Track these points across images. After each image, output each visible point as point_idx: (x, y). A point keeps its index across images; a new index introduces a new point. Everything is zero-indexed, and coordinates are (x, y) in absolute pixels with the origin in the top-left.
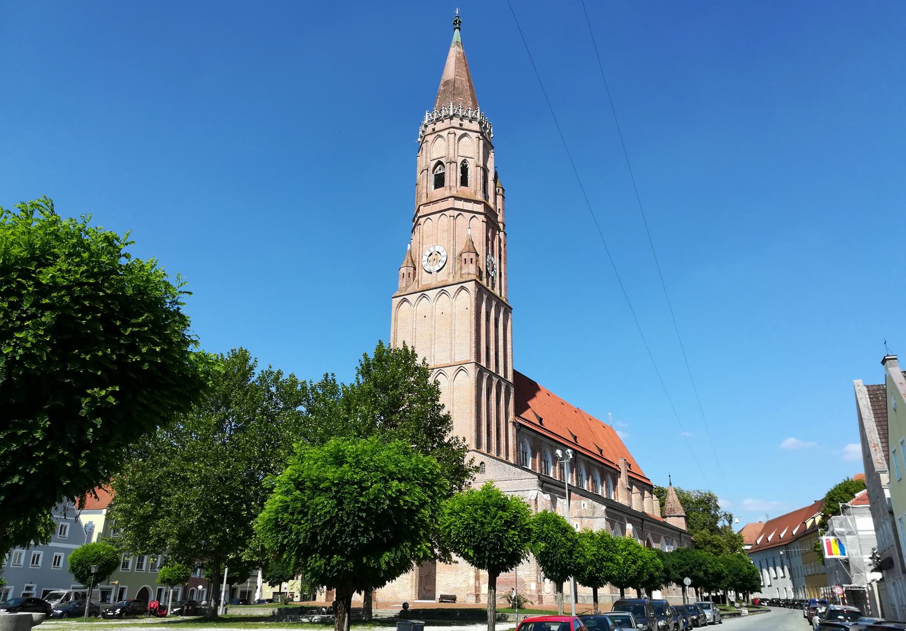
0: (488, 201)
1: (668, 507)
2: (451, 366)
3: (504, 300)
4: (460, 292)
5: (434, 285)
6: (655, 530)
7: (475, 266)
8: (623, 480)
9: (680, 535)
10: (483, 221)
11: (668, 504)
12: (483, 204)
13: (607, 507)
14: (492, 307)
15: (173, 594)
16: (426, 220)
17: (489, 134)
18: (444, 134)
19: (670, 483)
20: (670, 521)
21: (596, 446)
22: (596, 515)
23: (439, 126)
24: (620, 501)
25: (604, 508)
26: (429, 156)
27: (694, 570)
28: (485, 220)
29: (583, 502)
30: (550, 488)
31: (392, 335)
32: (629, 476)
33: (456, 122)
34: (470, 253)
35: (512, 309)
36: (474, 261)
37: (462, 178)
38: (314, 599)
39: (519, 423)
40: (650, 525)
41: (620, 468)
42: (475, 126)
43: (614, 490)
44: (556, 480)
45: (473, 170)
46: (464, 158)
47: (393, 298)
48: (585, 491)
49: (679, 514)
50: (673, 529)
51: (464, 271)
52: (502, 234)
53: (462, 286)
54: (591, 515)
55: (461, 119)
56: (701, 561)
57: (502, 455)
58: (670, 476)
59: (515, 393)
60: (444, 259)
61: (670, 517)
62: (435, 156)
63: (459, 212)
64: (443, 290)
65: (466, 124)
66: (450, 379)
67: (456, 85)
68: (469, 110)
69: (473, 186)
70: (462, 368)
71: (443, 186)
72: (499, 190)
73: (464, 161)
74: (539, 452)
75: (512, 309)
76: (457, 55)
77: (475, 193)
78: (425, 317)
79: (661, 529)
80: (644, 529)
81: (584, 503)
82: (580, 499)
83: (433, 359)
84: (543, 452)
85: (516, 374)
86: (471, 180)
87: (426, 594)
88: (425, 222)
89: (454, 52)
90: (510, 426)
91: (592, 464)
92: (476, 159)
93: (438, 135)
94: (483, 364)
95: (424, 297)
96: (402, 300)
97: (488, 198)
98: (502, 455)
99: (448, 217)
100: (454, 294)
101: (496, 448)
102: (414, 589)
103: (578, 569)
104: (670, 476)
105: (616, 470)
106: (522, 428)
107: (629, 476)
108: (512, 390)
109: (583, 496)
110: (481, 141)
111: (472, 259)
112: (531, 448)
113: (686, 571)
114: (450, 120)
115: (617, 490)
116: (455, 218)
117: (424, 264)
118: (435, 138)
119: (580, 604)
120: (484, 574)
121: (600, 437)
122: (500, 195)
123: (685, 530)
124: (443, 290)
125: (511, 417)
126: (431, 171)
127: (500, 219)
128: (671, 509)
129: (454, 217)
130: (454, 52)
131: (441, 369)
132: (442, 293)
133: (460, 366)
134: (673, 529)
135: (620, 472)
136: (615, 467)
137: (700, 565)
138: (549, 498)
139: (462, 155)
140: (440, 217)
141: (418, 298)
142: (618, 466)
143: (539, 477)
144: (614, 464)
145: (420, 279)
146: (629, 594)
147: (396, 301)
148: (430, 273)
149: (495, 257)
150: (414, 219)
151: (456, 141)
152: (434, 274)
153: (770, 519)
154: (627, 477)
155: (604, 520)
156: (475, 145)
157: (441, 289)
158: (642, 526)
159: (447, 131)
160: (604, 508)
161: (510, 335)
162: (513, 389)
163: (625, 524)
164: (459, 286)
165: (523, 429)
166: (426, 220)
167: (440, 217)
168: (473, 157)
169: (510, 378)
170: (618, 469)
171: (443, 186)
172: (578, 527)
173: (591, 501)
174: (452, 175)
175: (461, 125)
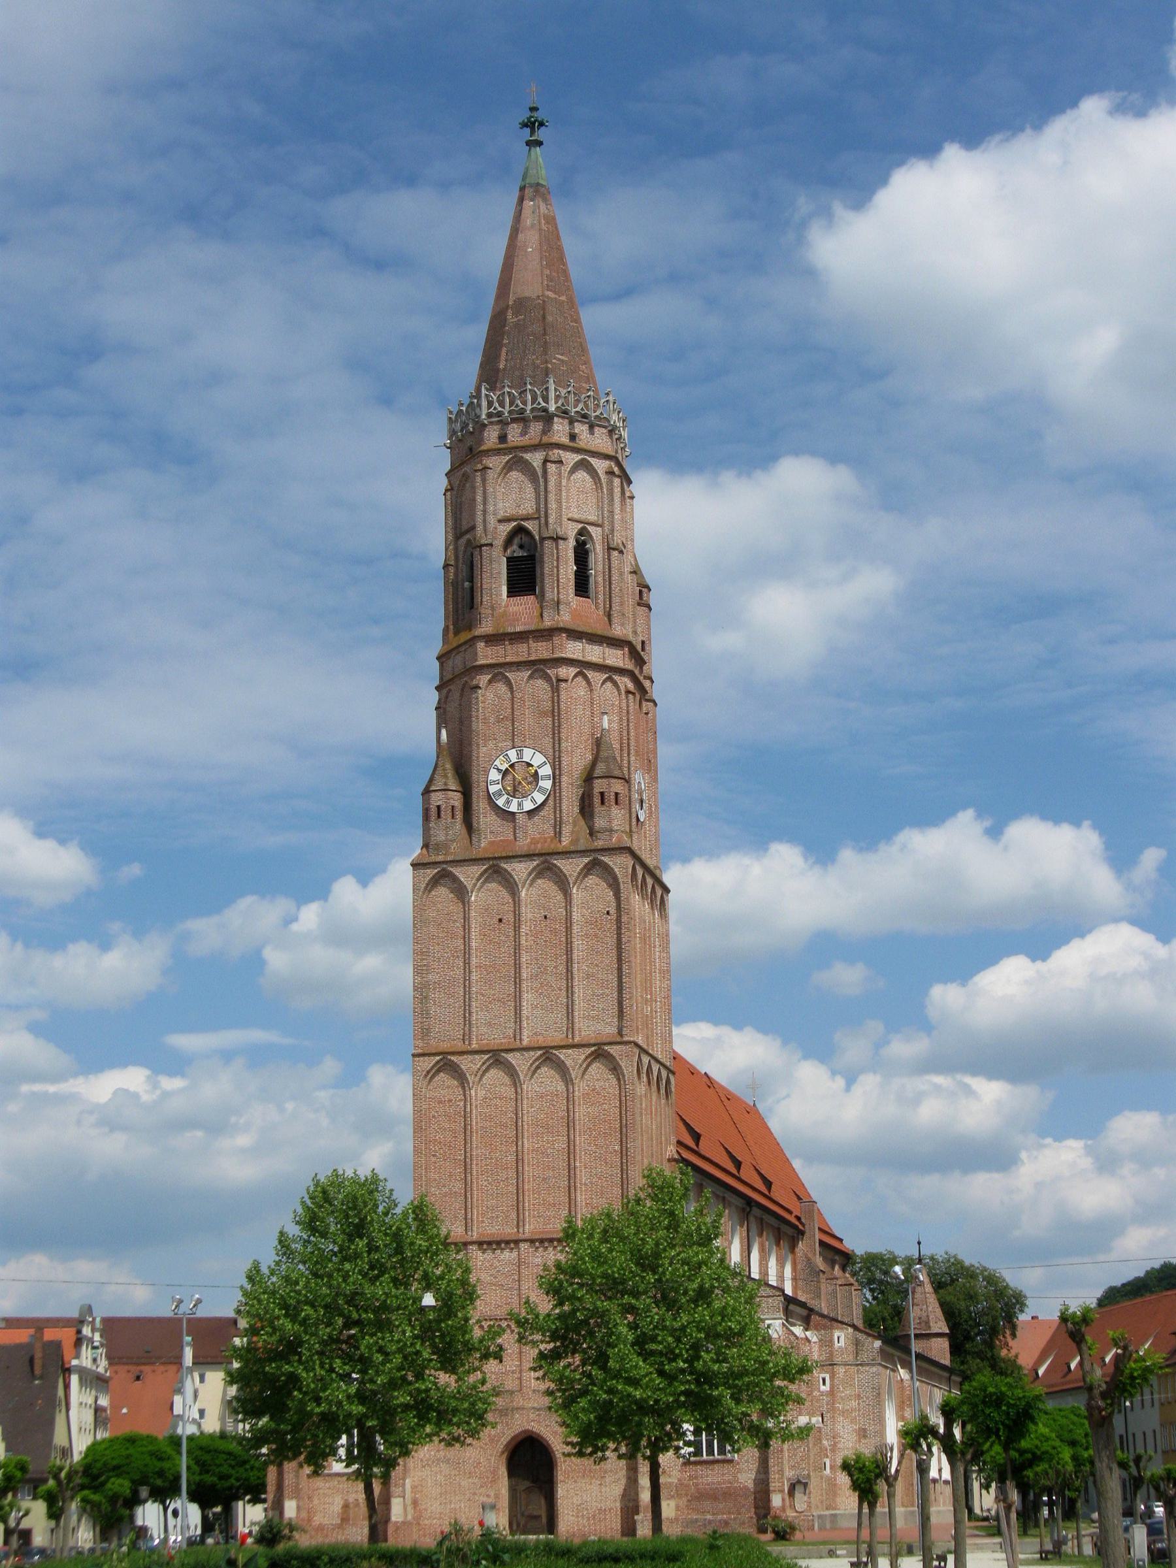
26: (491, 508)
37: (577, 574)
46: (580, 526)
51: (599, 823)
73: (582, 532)
78: (500, 920)
117: (493, 789)
175: (573, 437)
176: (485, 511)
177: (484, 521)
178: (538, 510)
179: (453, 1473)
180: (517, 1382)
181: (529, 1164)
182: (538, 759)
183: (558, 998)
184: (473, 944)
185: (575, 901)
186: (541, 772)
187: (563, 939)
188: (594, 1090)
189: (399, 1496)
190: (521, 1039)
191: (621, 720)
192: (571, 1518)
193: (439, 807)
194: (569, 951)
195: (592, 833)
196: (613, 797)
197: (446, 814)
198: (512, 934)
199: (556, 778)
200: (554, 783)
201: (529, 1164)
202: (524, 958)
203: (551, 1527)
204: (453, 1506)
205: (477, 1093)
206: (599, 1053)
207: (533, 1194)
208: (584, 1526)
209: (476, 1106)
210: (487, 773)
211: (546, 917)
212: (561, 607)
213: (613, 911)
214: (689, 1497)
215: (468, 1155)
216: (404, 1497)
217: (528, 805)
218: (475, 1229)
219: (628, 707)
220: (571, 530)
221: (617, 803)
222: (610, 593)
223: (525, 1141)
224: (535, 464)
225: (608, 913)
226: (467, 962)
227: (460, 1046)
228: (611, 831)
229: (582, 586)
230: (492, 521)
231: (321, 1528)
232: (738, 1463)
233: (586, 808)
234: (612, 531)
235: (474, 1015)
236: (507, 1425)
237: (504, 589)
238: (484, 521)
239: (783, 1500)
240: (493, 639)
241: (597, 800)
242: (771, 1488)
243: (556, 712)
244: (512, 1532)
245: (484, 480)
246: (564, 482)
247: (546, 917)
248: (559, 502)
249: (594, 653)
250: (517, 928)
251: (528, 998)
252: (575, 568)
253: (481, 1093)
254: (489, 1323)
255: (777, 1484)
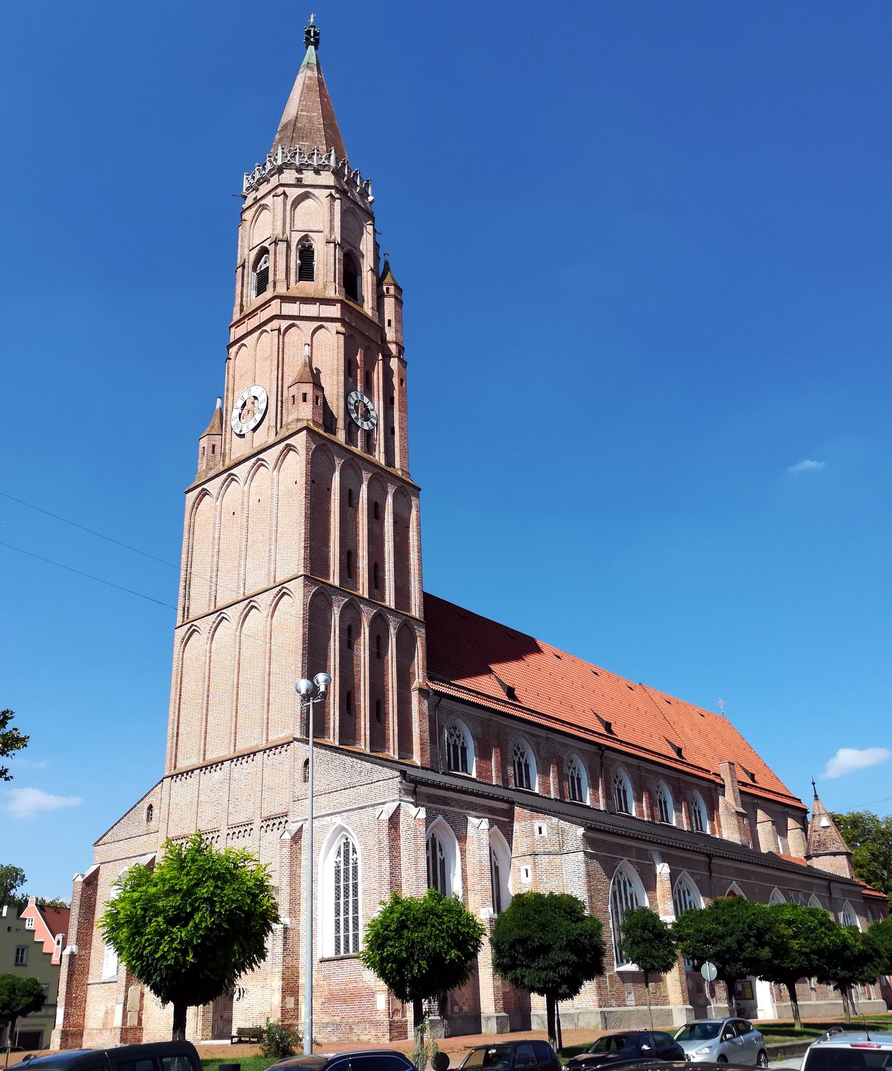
0: (362, 307)
1: (813, 839)
2: (266, 591)
3: (400, 473)
4: (285, 456)
6: (753, 878)
7: (311, 406)
8: (728, 801)
9: (829, 888)
10: (338, 333)
11: (814, 834)
12: (339, 305)
13: (588, 829)
14: (334, 471)
15: (220, 1038)
16: (239, 349)
17: (364, 194)
18: (268, 201)
19: (816, 796)
20: (822, 864)
21: (669, 742)
22: (566, 849)
23: (264, 188)
24: (725, 836)
25: (581, 831)
27: (747, 944)
28: (342, 330)
29: (537, 824)
30: (445, 798)
31: (184, 556)
32: (741, 792)
33: (289, 176)
34: (301, 385)
35: (420, 490)
36: (310, 397)
38: (479, 1032)
39: (434, 690)
40: (737, 868)
41: (722, 780)
42: (327, 178)
43: (712, 819)
44: (550, 799)
47: (187, 492)
48: (634, 818)
49: (834, 850)
50: (843, 883)
52: (394, 363)
53: (287, 445)
54: (556, 848)
55: (299, 171)
56: (760, 923)
57: (391, 750)
58: (814, 784)
59: (426, 637)
60: (263, 406)
61: (818, 856)
62: (257, 241)
63: (290, 322)
64: (259, 460)
65: (309, 177)
66: (265, 613)
67: (299, 125)
68: (313, 154)
69: (321, 277)
70: (284, 590)
72: (388, 289)
73: (305, 238)
74: (496, 747)
75: (420, 490)
76: (306, 82)
77: (325, 288)
79: (774, 875)
80: (713, 875)
81: (540, 825)
82: (532, 818)
83: (242, 585)
84: (511, 745)
85: (429, 600)
86: (318, 269)
87: (223, 1027)
88: (237, 353)
89: (304, 77)
90: (415, 697)
91: (647, 771)
92: (327, 231)
93: (260, 206)
94: (390, 600)
95: (233, 480)
96: (200, 493)
97: (363, 301)
98: (391, 750)
99: (270, 331)
100: (274, 461)
101: (368, 737)
102: (200, 1018)
104: (814, 784)
105: (713, 782)
106: (443, 699)
107: (741, 792)
108: (421, 634)
109: (537, 812)
110: (338, 202)
112: (475, 737)
113: (729, 948)
114: (279, 175)
115: (718, 817)
116: (282, 333)
119: (486, 1036)
120: (783, 987)
121: (686, 729)
122: (391, 296)
123: (849, 877)
124: (259, 460)
125: (419, 678)
126: (251, 267)
127: (390, 334)
128: (819, 842)
129: (279, 330)
130: (304, 77)
131: (252, 599)
132: (259, 467)
133: (280, 587)
134: (843, 883)
135: (723, 786)
136: (712, 777)
137: (760, 934)
138: (422, 814)
139: (300, 229)
140: (258, 339)
142: (719, 775)
143: (403, 774)
144: (710, 772)
145: (227, 451)
146: (669, 1004)
147: (191, 496)
148: (242, 436)
149: (376, 399)
151: (288, 207)
152: (248, 436)
154: (738, 793)
155: (581, 856)
156: (326, 209)
157: (256, 458)
158: (710, 868)
160: (581, 831)
161: (415, 534)
162: (423, 631)
163: (654, 865)
164: (283, 445)
165: (445, 702)
166: (239, 349)
167: (258, 339)
168: (322, 229)
169: (416, 610)
170: (718, 781)
173: (555, 820)
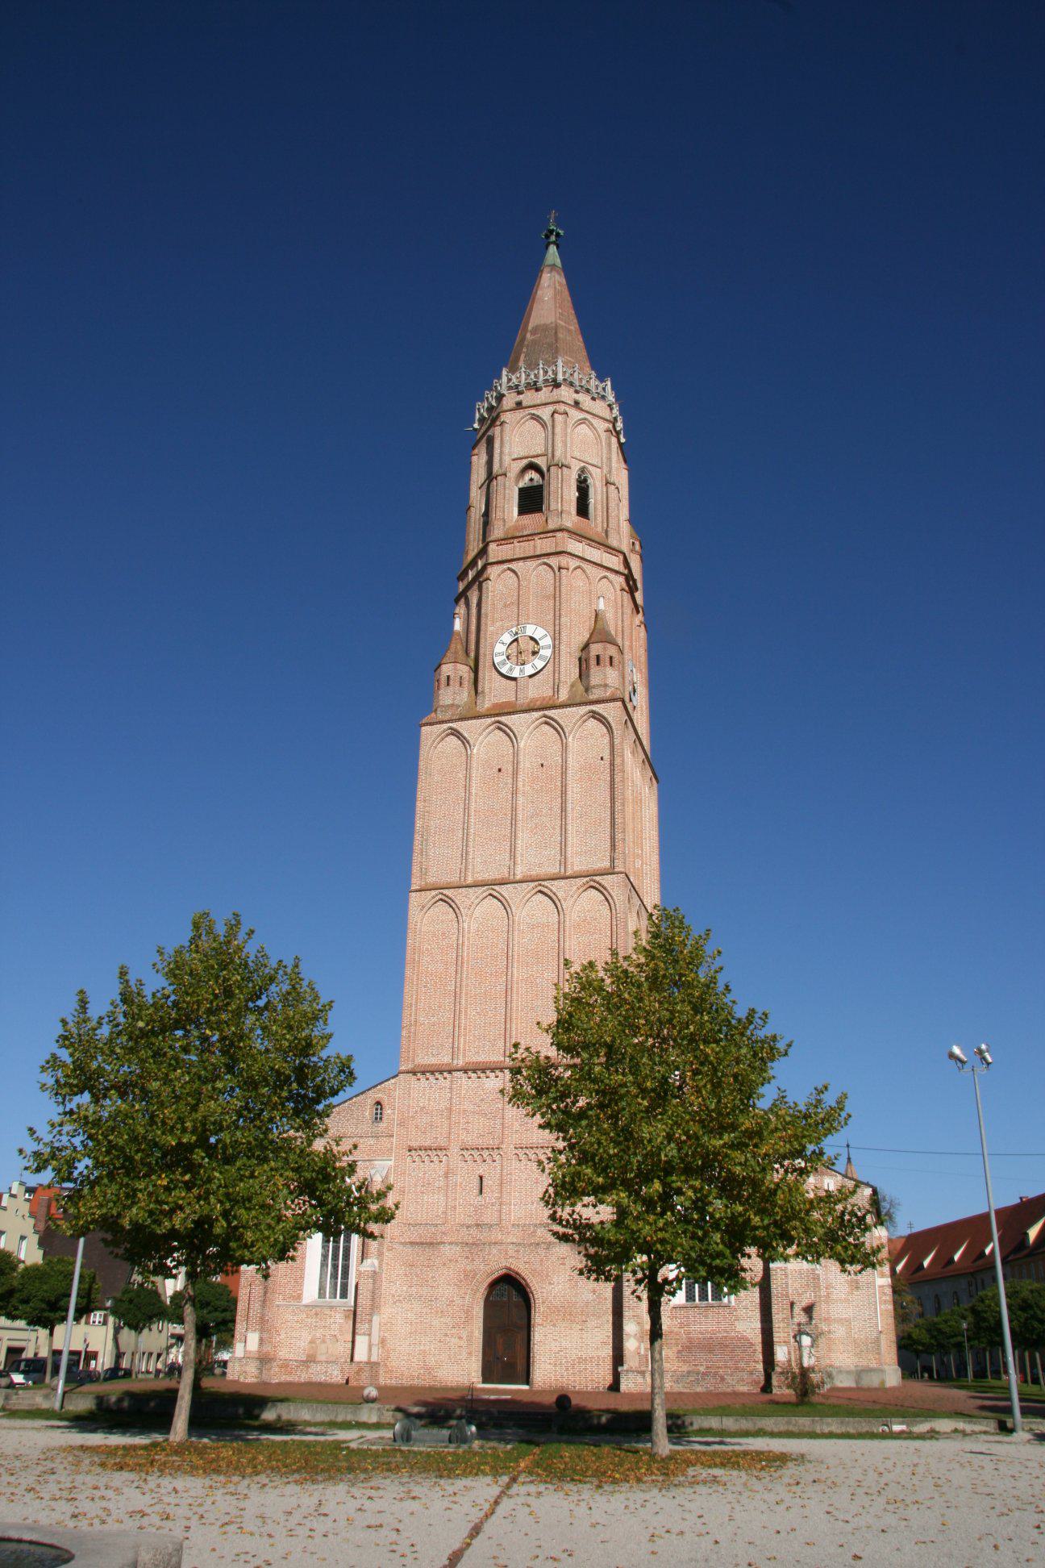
5: (523, 701)
16: (503, 572)
23: (528, 398)
37: (579, 499)
45: (599, 490)
46: (583, 464)
69: (599, 519)
70: (592, 883)
71: (540, 510)
73: (583, 470)
78: (500, 770)
103: (332, 1226)
111: (611, 658)
117: (497, 660)
118: (522, 418)
141: (484, 730)
150: (465, 573)
153: (914, 1230)
159: (550, 409)
171: (540, 510)
172: (595, 1220)
174: (561, 496)
176: (501, 453)
177: (501, 460)
178: (546, 449)
179: (424, 1311)
180: (496, 1215)
181: (518, 993)
182: (538, 633)
183: (552, 837)
184: (473, 791)
185: (570, 749)
186: (542, 652)
187: (559, 784)
188: (584, 920)
189: (364, 1334)
190: (514, 874)
191: (616, 612)
192: (549, 1366)
193: (448, 677)
194: (564, 793)
195: (587, 690)
196: (608, 660)
197: (454, 683)
198: (510, 781)
199: (555, 648)
200: (554, 652)
201: (518, 993)
202: (521, 800)
203: (527, 1381)
204: (422, 1348)
205: (470, 924)
206: (592, 879)
207: (521, 1023)
208: (562, 1376)
209: (468, 938)
210: (493, 647)
211: (542, 765)
212: (564, 515)
213: (607, 756)
214: (680, 1348)
215: (458, 985)
216: (370, 1335)
217: (529, 670)
218: (461, 1057)
219: (622, 601)
220: (576, 467)
221: (611, 665)
222: (607, 509)
223: (515, 971)
224: (544, 418)
225: (602, 759)
226: (467, 809)
227: (454, 879)
228: (606, 686)
229: (583, 509)
230: (507, 459)
231: (285, 1365)
232: (735, 1310)
233: (583, 664)
234: (610, 472)
235: (472, 817)
236: (484, 1261)
237: (516, 510)
238: (501, 460)
239: (789, 1353)
240: (506, 540)
241: (593, 662)
242: (775, 1339)
243: (556, 596)
244: (485, 1380)
245: (502, 431)
246: (569, 430)
247: (542, 765)
248: (565, 443)
249: (595, 554)
250: (515, 774)
251: (523, 838)
252: (577, 494)
253: (474, 926)
254: (180, 1043)
255: (782, 1335)
